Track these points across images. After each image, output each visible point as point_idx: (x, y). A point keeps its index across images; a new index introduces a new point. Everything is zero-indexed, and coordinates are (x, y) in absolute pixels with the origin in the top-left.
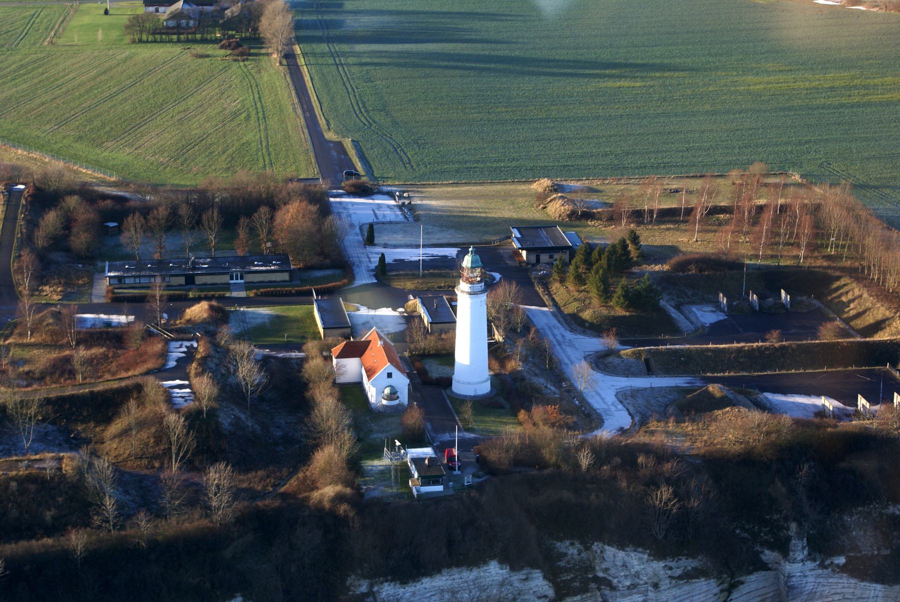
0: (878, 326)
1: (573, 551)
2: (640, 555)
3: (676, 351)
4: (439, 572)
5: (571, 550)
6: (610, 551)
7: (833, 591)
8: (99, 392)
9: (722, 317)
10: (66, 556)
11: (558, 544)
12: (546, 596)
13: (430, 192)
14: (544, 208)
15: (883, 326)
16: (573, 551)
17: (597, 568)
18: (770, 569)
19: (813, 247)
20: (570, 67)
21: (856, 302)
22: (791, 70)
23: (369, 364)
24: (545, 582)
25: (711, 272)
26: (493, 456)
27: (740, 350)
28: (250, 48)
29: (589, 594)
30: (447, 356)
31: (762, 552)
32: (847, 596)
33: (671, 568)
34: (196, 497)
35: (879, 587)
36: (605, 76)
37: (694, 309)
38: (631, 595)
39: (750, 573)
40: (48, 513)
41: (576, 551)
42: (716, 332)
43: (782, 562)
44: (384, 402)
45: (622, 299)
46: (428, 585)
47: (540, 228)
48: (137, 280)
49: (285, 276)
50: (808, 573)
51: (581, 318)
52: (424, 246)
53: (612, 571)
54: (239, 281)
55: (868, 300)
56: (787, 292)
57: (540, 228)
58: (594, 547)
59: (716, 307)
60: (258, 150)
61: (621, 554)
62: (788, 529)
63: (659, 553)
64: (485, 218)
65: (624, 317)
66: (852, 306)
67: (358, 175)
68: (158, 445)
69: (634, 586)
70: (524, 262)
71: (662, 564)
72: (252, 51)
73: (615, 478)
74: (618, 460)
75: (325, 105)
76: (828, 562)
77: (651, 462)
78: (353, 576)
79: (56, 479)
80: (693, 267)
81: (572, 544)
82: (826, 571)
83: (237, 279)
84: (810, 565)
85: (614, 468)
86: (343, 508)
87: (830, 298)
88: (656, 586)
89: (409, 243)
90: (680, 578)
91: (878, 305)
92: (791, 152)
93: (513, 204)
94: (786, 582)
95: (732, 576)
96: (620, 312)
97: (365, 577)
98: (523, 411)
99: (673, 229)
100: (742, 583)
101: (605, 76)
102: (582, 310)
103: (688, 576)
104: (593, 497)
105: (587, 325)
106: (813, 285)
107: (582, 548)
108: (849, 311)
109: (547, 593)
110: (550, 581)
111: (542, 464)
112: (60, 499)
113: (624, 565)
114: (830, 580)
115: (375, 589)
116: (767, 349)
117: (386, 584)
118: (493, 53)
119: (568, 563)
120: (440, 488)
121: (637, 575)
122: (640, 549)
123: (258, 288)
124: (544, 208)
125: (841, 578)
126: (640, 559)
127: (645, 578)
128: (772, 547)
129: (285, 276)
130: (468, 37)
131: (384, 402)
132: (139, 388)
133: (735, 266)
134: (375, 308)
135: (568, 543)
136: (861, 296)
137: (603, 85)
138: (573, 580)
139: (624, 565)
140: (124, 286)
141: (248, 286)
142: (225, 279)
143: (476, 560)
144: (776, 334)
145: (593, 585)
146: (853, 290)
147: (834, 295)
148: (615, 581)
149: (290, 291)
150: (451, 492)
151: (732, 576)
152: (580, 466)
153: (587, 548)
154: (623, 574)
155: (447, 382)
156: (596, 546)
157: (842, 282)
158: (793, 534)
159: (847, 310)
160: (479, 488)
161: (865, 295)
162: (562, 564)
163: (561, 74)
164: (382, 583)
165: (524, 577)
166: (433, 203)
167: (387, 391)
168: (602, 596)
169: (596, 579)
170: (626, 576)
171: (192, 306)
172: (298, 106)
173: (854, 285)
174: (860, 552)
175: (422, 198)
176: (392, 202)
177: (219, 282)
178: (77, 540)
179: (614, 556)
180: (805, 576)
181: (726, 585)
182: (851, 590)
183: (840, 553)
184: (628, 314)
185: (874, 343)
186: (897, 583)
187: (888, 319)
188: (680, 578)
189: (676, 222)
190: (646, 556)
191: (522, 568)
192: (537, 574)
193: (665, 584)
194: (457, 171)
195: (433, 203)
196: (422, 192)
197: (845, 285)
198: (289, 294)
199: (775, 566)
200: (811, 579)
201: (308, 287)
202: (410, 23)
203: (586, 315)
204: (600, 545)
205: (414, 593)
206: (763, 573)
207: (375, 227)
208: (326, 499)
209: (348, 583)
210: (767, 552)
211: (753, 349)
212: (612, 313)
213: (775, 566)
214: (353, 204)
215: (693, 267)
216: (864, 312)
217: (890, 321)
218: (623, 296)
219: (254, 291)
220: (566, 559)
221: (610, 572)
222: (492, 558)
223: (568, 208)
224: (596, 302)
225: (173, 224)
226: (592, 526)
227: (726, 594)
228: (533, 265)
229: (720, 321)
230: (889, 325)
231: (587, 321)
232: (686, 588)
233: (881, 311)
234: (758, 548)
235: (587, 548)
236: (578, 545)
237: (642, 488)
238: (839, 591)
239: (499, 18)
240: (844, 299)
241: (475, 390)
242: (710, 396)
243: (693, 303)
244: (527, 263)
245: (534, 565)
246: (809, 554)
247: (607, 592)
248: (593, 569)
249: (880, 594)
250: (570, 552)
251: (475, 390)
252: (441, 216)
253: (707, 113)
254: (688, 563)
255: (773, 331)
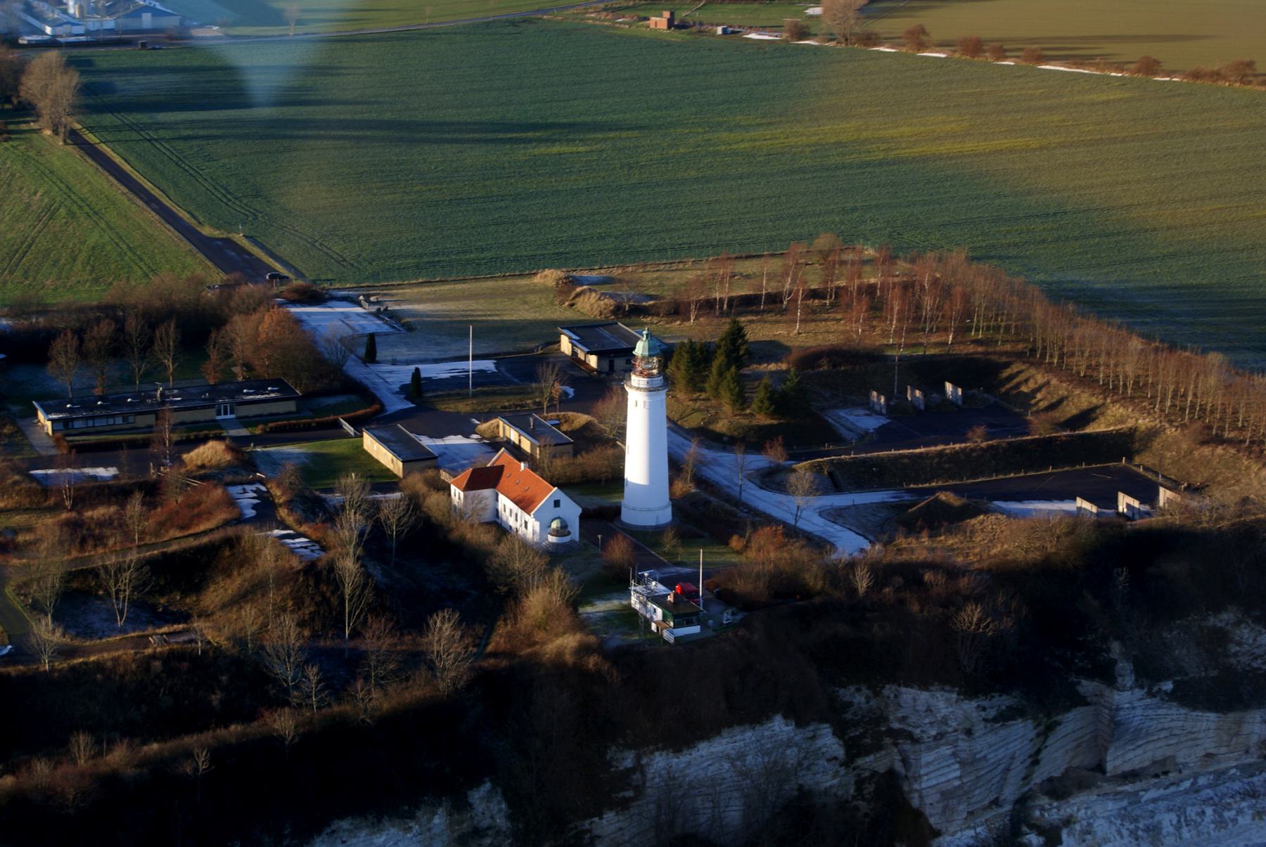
0: (1086, 416)
1: (859, 699)
2: (947, 695)
3: (864, 461)
4: (719, 733)
5: (857, 697)
6: (909, 695)
7: (1160, 726)
8: (174, 554)
9: (883, 421)
10: (272, 742)
11: (842, 691)
12: (835, 758)
13: (403, 294)
14: (572, 305)
15: (1093, 416)
16: (859, 699)
17: (892, 718)
18: (1087, 704)
19: (963, 330)
20: (474, 131)
21: (1044, 391)
22: (770, 124)
23: (518, 493)
24: (835, 740)
25: (849, 367)
26: (741, 586)
27: (941, 454)
28: (6, 124)
29: (883, 753)
30: (616, 480)
31: (1079, 683)
32: (1175, 732)
33: (984, 709)
34: (416, 660)
35: (1212, 716)
36: (530, 141)
37: (842, 413)
38: (938, 747)
39: (1068, 710)
40: (213, 697)
41: (863, 699)
42: (884, 437)
43: (1107, 692)
44: (552, 539)
45: (767, 403)
46: (704, 752)
47: (598, 326)
48: (90, 423)
49: (290, 406)
50: (1136, 704)
51: (713, 432)
52: (475, 357)
53: (913, 719)
54: (229, 416)
55: (1060, 388)
56: (956, 384)
57: (598, 326)
58: (886, 692)
59: (869, 409)
60: (120, 255)
61: (924, 695)
62: (1108, 650)
63: (971, 689)
64: (502, 321)
65: (772, 426)
66: (1039, 396)
67: (283, 278)
68: (299, 609)
69: (940, 737)
70: (593, 370)
71: (974, 704)
72: (11, 127)
73: (901, 602)
74: (899, 580)
75: (171, 192)
76: (1155, 689)
77: (941, 579)
78: (614, 748)
79: (211, 653)
80: (824, 361)
81: (858, 690)
82: (1155, 700)
83: (226, 413)
84: (1139, 693)
85: (898, 590)
86: (592, 661)
87: (1003, 390)
88: (969, 732)
89: (422, 357)
90: (995, 720)
91: (1077, 392)
92: (842, 223)
93: (526, 303)
94: (1113, 718)
95: (1049, 715)
96: (763, 420)
97: (628, 747)
98: (735, 537)
99: (759, 321)
100: (1059, 723)
101: (530, 141)
102: (715, 419)
103: (1004, 717)
104: (876, 628)
105: (725, 439)
106: (979, 373)
107: (870, 694)
108: (1036, 404)
109: (836, 754)
110: (840, 738)
111: (807, 594)
112: (224, 678)
113: (929, 710)
114: (1160, 712)
115: (644, 761)
116: (972, 450)
117: (657, 754)
118: (357, 117)
119: (855, 714)
120: (696, 629)
121: (945, 721)
122: (947, 688)
123: (266, 423)
124: (572, 305)
125: (1170, 708)
126: (947, 700)
127: (954, 724)
128: (1090, 676)
129: (290, 406)
130: (307, 98)
131: (552, 539)
132: (231, 542)
133: (874, 357)
134: (441, 436)
135: (852, 689)
136: (1048, 383)
137: (536, 151)
138: (862, 736)
139: (929, 710)
140: (72, 432)
141: (245, 422)
142: (210, 414)
143: (756, 717)
144: (980, 430)
145: (888, 741)
146: (1033, 376)
147: (1008, 386)
148: (918, 731)
149: (309, 424)
150: (710, 633)
151: (1049, 715)
152: (856, 590)
153: (877, 694)
154: (927, 721)
155: (617, 511)
156: (889, 690)
157: (1015, 368)
158: (1116, 657)
159: (1033, 402)
160: (744, 623)
161: (1054, 381)
162: (848, 716)
163: (510, 140)
164: (652, 753)
165: (811, 734)
166: (416, 307)
167: (555, 525)
168: (901, 752)
169: (891, 733)
170: (931, 723)
171: (192, 450)
172: (131, 196)
173: (1033, 371)
174: (1186, 674)
175: (398, 302)
176: (359, 310)
177: (251, 414)
178: (283, 723)
179: (915, 700)
180: (1134, 708)
181: (1042, 728)
182: (1180, 724)
183: (1168, 677)
184: (775, 422)
185: (1090, 435)
186: (1260, 706)
187: (1096, 407)
188: (995, 720)
189: (757, 313)
190: (954, 696)
191: (808, 724)
192: (826, 730)
193: (979, 729)
194: (417, 266)
195: (416, 307)
196: (392, 295)
197: (1019, 372)
198: (308, 428)
199: (1095, 699)
200: (1139, 712)
201: (332, 417)
202: (207, 82)
203: (721, 426)
204: (894, 687)
205: (689, 764)
206: (1082, 709)
207: (377, 339)
208: (567, 651)
209: (608, 757)
210: (1084, 682)
211: (957, 452)
212: (754, 423)
213: (1095, 699)
214: (309, 314)
215: (824, 361)
216: (1060, 402)
217: (1102, 409)
218: (769, 399)
219: (261, 426)
220: (852, 709)
221: (910, 721)
222: (775, 712)
223: (609, 302)
224: (727, 408)
225: (117, 348)
226: (887, 665)
227: (1042, 738)
228: (607, 374)
229: (884, 426)
230: (1102, 414)
231: (724, 435)
232: (1002, 733)
233: (1083, 399)
234: (1073, 678)
235: (877, 694)
236: (865, 691)
237: (940, 610)
238: (1166, 725)
239: (335, 71)
240: (1024, 389)
241: (657, 518)
242: (946, 507)
243: (836, 407)
244: (599, 371)
245: (823, 720)
246: (1136, 680)
247: (907, 746)
248: (886, 719)
249: (1213, 726)
250: (856, 701)
251: (657, 518)
252: (442, 323)
253: (697, 180)
254: (1003, 701)
255: (975, 428)
